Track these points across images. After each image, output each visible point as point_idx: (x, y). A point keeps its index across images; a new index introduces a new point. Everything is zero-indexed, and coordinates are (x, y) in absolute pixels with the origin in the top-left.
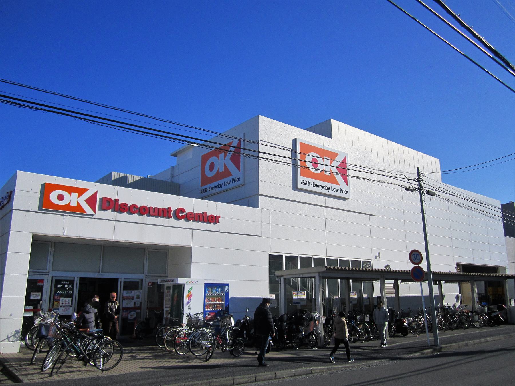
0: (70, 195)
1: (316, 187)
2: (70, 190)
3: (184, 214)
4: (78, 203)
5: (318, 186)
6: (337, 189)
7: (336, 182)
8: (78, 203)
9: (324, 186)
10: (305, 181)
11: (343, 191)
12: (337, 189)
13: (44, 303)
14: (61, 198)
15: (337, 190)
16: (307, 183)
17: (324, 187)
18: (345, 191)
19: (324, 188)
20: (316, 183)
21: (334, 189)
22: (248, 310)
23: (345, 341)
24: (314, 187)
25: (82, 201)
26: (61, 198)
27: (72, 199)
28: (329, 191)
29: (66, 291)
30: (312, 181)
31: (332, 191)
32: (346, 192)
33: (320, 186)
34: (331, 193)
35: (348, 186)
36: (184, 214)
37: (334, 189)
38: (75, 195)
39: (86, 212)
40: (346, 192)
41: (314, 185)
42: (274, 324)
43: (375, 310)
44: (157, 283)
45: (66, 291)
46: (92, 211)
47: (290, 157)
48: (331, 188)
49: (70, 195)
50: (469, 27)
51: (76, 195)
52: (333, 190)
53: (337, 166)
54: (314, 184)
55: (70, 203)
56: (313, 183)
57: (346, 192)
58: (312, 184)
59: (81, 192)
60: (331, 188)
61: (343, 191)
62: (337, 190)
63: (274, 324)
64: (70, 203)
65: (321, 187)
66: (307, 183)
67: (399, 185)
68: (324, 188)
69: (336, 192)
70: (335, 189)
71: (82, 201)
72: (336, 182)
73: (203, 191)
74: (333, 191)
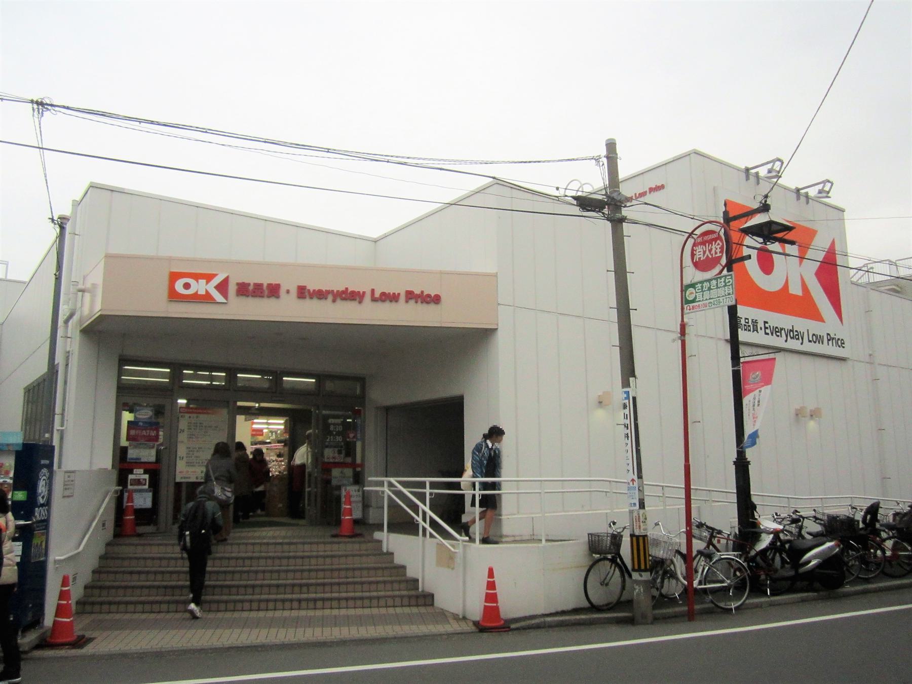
0: (198, 282)
1: (772, 334)
2: (197, 277)
4: (207, 291)
5: (776, 332)
6: (820, 336)
7: (816, 316)
8: (207, 291)
9: (791, 330)
10: (746, 319)
11: (834, 341)
12: (820, 336)
14: (187, 286)
15: (818, 339)
16: (750, 324)
18: (839, 339)
19: (792, 336)
20: (772, 324)
25: (211, 288)
26: (187, 286)
27: (200, 287)
28: (802, 344)
29: (332, 437)
31: (810, 341)
32: (839, 342)
33: (782, 329)
34: (808, 347)
37: (814, 335)
38: (203, 282)
39: (215, 300)
41: (767, 328)
43: (686, 618)
44: (694, 580)
45: (332, 437)
46: (223, 298)
48: (806, 334)
49: (198, 282)
51: (204, 281)
52: (811, 339)
53: (821, 260)
54: (767, 325)
55: (197, 292)
57: (839, 342)
59: (209, 277)
60: (806, 334)
62: (818, 339)
64: (197, 292)
65: (783, 331)
66: (750, 324)
67: (769, 192)
68: (792, 336)
69: (819, 343)
71: (211, 288)
72: (816, 316)
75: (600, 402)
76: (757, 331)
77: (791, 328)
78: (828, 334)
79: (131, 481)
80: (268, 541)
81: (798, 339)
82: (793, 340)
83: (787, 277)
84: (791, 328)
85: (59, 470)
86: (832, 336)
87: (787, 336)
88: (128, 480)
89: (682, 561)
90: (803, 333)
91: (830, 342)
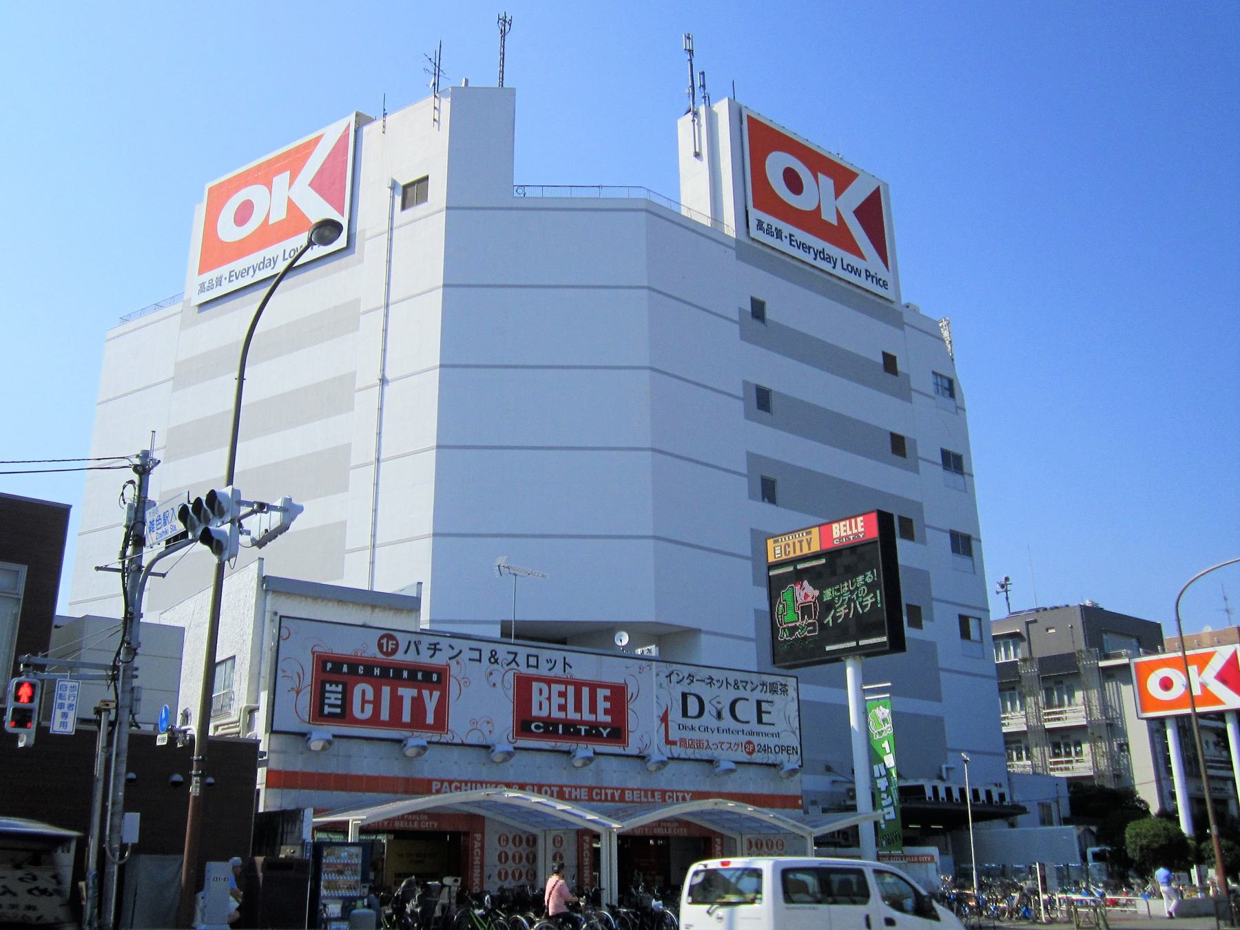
1: (799, 248)
3: (537, 723)
6: (857, 269)
9: (820, 252)
12: (857, 269)
13: (604, 891)
15: (857, 272)
17: (822, 255)
19: (822, 257)
21: (849, 267)
22: (702, 844)
23: (658, 648)
24: (794, 246)
30: (787, 229)
32: (881, 282)
33: (810, 248)
35: (888, 270)
36: (537, 723)
40: (881, 283)
42: (1210, 829)
47: (741, 395)
50: (862, 643)
52: (845, 267)
54: (792, 238)
56: (791, 235)
57: (881, 282)
58: (788, 237)
59: (293, 162)
60: (839, 263)
61: (874, 279)
62: (857, 272)
63: (1210, 829)
65: (811, 250)
68: (822, 257)
70: (852, 268)
73: (206, 285)
74: (845, 270)
75: (908, 307)
76: (781, 239)
77: (822, 250)
78: (866, 271)
79: (758, 891)
80: (1036, 828)
81: (830, 262)
82: (823, 261)
83: (837, 208)
84: (822, 250)
85: (1169, 633)
86: (872, 273)
87: (816, 255)
88: (189, 798)
89: (1175, 670)
90: (836, 259)
91: (870, 279)
